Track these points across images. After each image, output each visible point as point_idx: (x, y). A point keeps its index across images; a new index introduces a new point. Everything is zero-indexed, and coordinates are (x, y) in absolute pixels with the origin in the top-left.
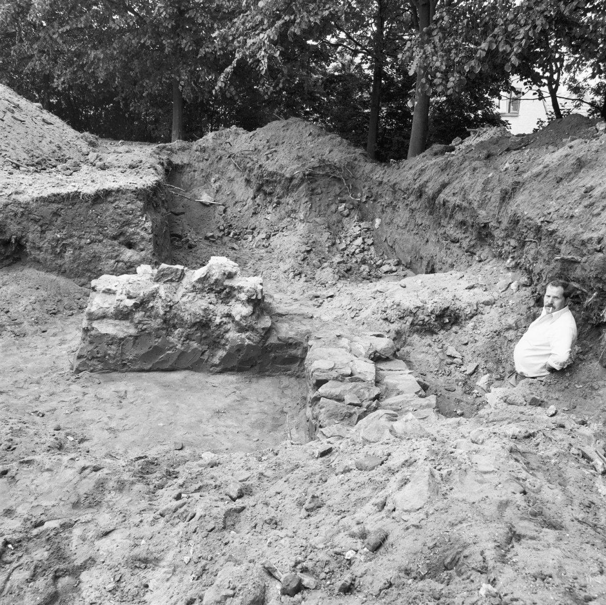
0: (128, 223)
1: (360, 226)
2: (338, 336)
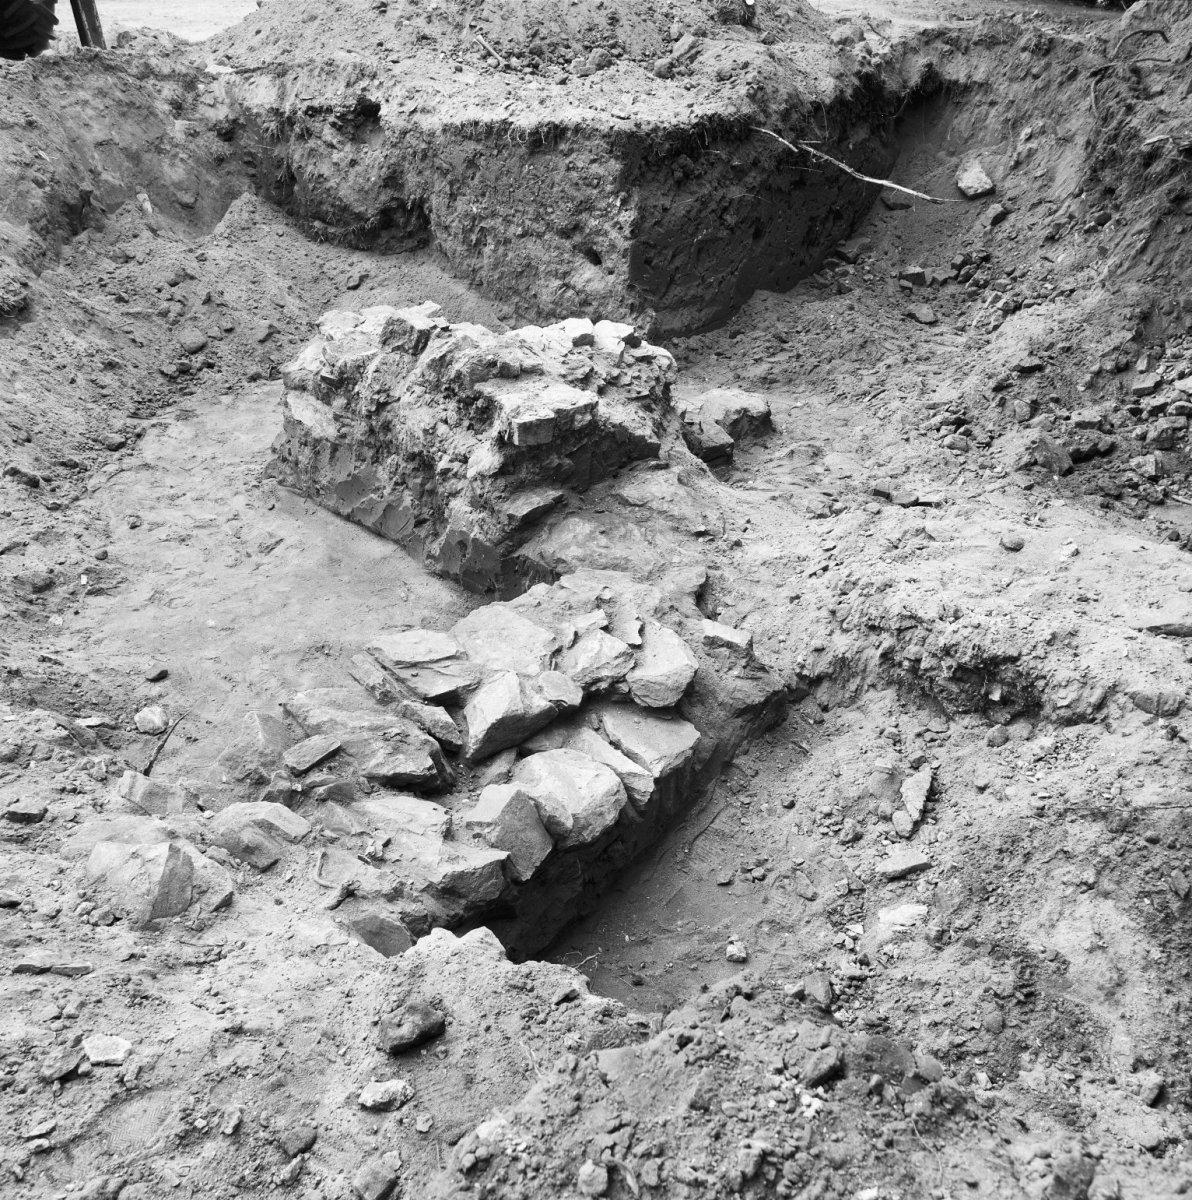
0: (586, 206)
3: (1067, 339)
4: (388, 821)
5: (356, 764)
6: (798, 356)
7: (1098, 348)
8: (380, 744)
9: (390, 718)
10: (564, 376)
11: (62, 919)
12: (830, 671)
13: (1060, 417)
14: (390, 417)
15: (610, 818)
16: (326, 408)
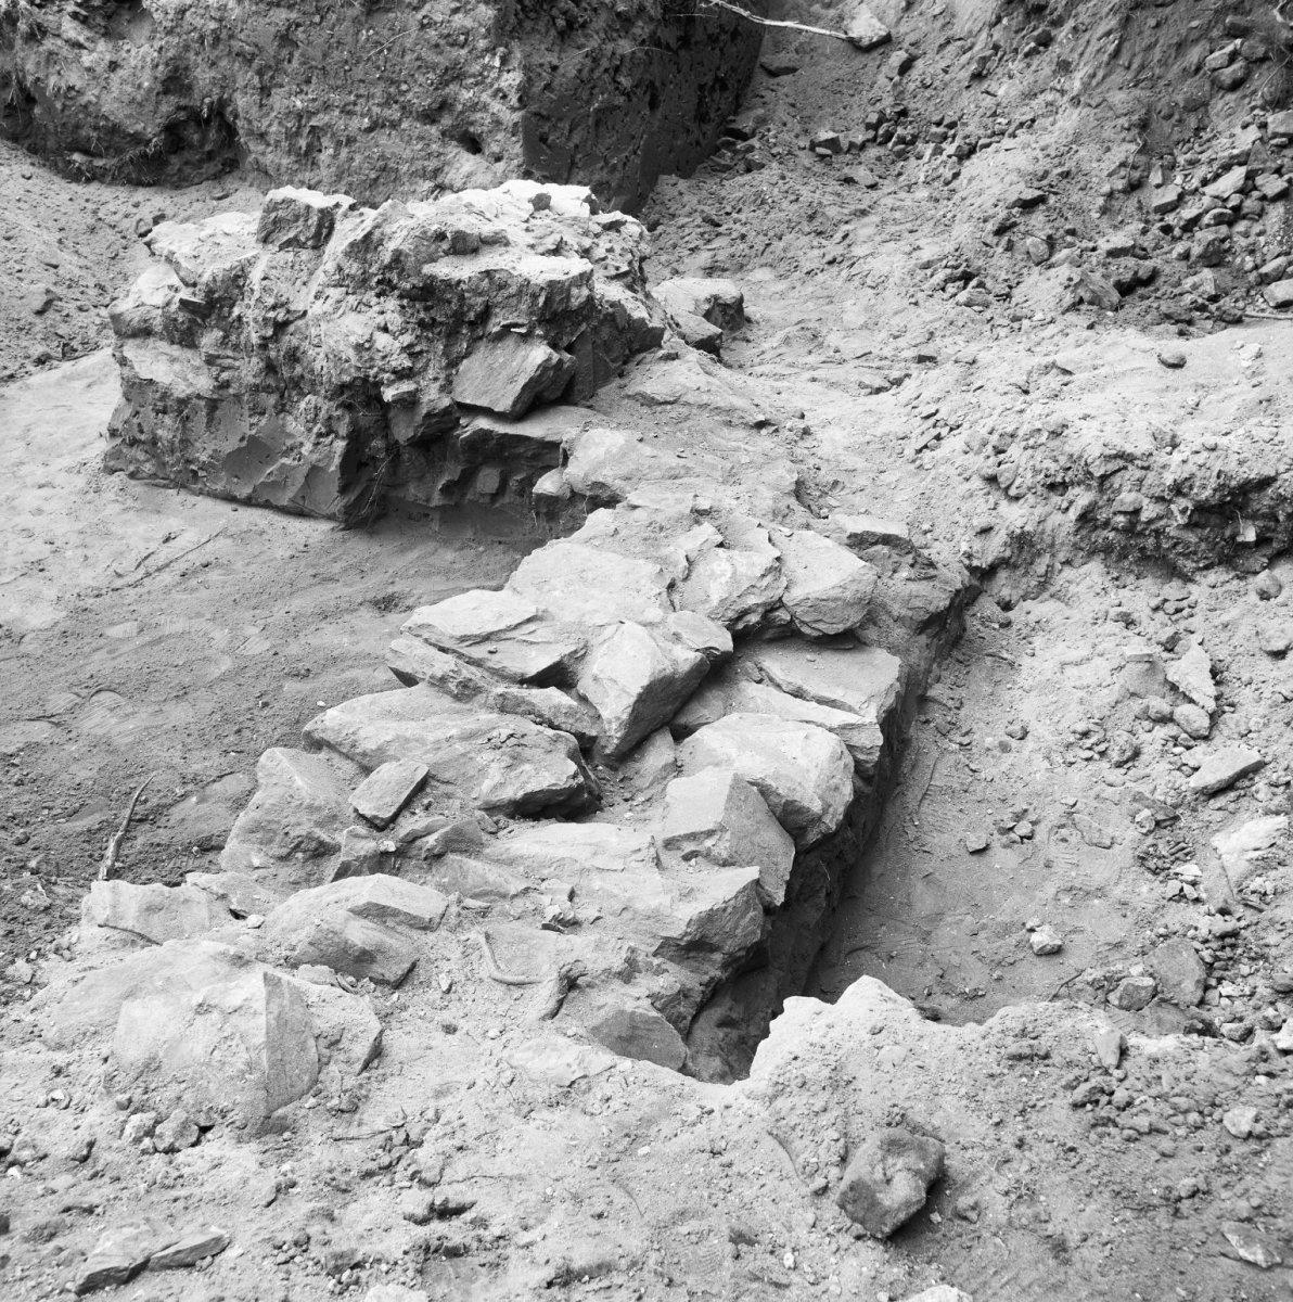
0: (454, 74)
1: (1263, 126)
3: (1060, 165)
4: (561, 863)
5: (459, 793)
6: (743, 237)
7: (1104, 164)
8: (487, 756)
9: (486, 717)
10: (532, 247)
11: (103, 1157)
12: (1008, 554)
13: (1086, 249)
14: (295, 342)
15: (847, 792)
16: (189, 353)
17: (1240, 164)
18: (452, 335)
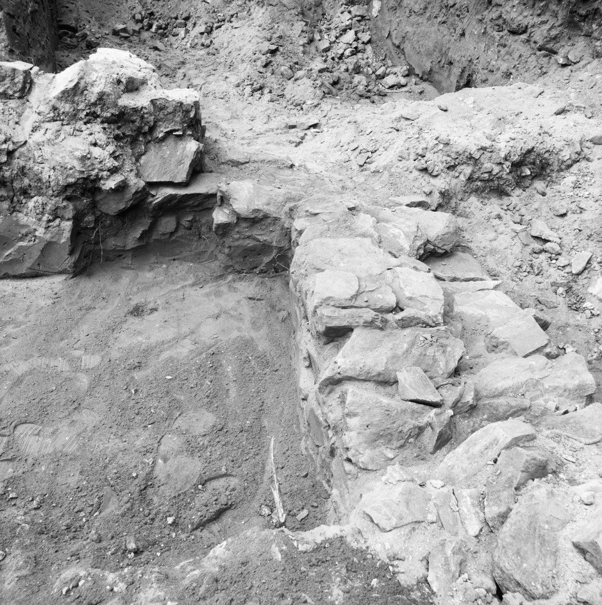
1: (350, 12)
2: (350, 209)
14: (22, 163)
17: (350, 29)
18: (134, 141)
